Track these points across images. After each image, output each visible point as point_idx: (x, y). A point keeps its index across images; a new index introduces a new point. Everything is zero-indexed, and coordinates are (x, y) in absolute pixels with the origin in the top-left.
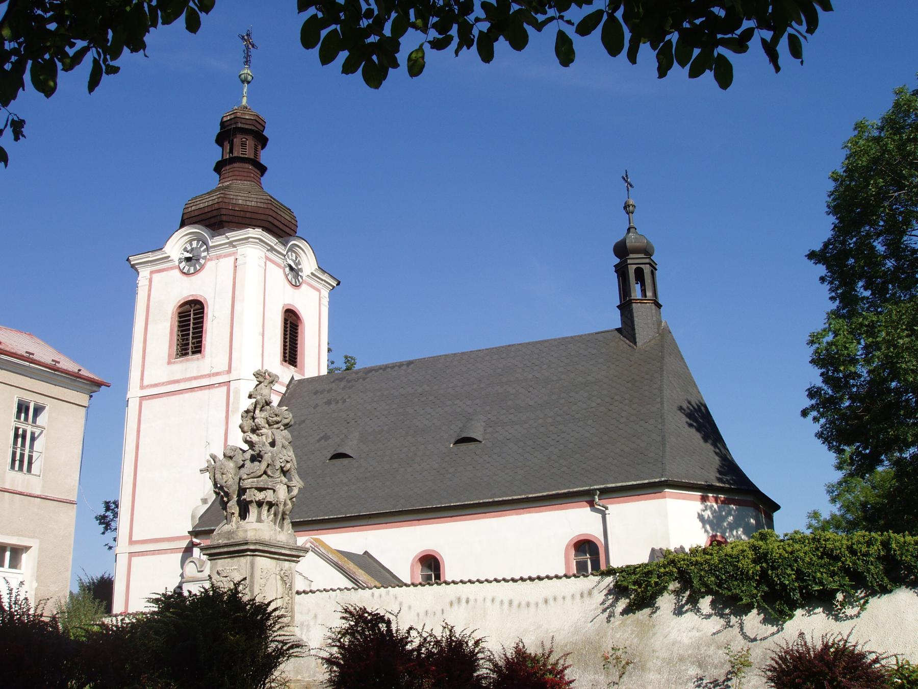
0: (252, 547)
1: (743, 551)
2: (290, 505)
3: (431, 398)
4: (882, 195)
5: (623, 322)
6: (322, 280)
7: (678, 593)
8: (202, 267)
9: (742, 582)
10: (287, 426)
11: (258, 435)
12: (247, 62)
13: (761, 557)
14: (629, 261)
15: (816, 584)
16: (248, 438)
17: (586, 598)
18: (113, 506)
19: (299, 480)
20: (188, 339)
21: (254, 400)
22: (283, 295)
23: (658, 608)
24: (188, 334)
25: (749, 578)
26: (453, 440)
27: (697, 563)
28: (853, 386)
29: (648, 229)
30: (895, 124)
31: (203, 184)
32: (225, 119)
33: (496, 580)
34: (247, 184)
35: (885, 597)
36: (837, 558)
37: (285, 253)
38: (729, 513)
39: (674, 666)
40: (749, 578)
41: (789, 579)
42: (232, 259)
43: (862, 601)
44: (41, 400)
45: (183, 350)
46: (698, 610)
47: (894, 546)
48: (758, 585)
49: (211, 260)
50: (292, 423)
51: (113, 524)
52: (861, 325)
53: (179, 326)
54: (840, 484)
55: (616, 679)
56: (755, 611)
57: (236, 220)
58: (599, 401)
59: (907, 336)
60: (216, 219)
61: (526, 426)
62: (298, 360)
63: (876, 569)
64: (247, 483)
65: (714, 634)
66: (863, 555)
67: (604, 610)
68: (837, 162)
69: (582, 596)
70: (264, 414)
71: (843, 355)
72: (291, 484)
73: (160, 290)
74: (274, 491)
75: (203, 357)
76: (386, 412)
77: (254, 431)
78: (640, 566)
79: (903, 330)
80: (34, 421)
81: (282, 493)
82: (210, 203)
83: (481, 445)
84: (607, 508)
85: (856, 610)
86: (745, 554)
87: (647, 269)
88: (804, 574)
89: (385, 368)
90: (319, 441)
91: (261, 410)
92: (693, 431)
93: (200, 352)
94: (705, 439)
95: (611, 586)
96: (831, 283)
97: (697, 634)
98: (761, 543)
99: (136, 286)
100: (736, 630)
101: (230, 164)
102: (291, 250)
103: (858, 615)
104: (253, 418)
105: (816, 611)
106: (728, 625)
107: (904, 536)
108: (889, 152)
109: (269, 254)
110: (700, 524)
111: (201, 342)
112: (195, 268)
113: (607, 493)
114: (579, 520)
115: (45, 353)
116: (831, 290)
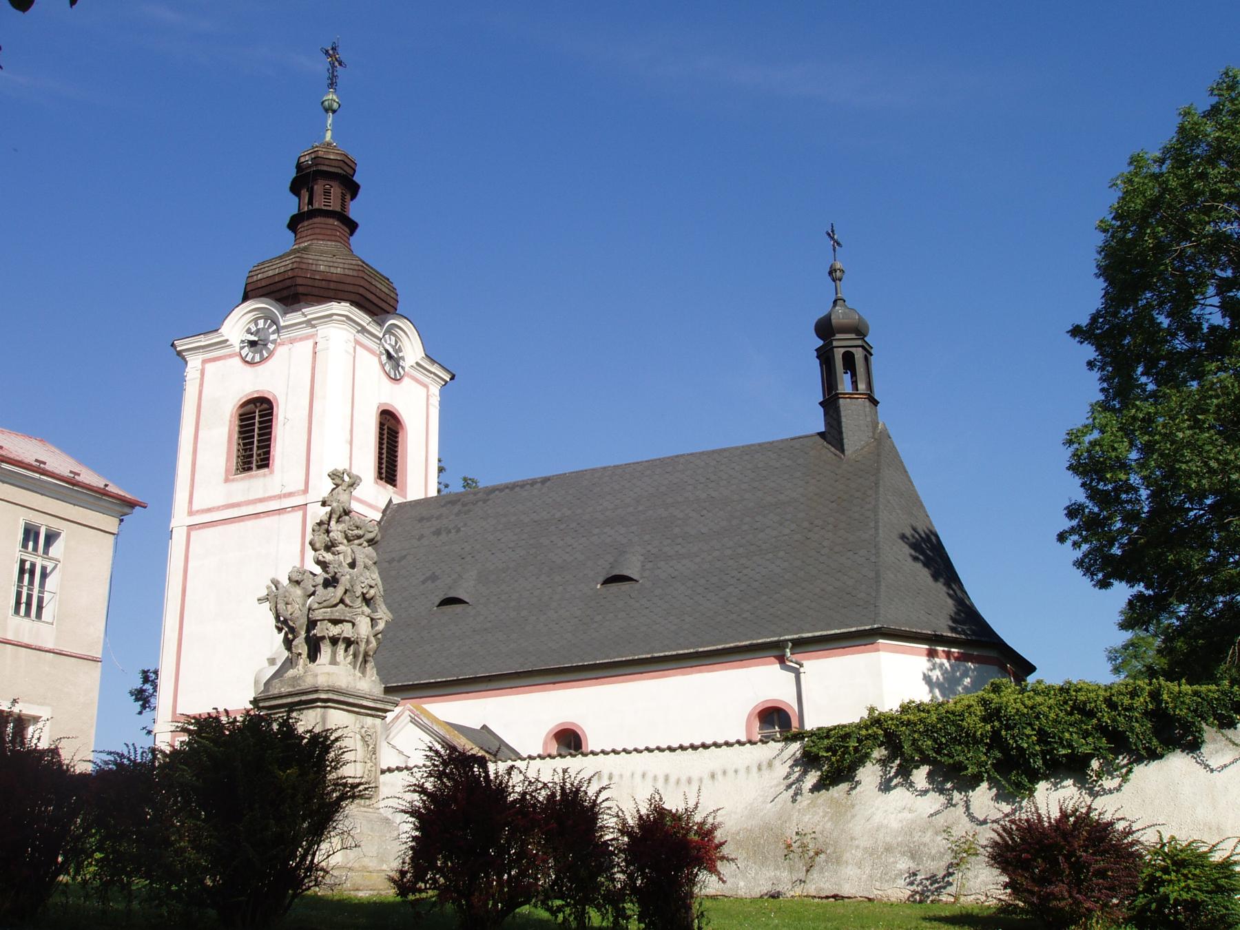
0: (323, 696)
1: (970, 706)
2: (374, 644)
3: (573, 525)
4: (1161, 249)
5: (827, 424)
6: (431, 372)
7: (884, 762)
8: (271, 353)
9: (967, 746)
10: (371, 542)
11: (333, 554)
12: (332, 84)
13: (992, 714)
14: (835, 344)
15: (1064, 747)
16: (321, 558)
17: (765, 772)
18: (153, 676)
19: (386, 611)
20: (251, 449)
21: (328, 509)
22: (378, 391)
23: (858, 783)
24: (252, 443)
25: (976, 742)
26: (601, 579)
27: (909, 723)
28: (1127, 502)
29: (860, 302)
30: (1180, 155)
31: (275, 245)
32: (302, 160)
33: (648, 750)
34: (330, 245)
35: (1154, 765)
36: (1091, 714)
37: (381, 335)
38: (965, 674)
39: (879, 857)
40: (976, 742)
41: (1027, 741)
42: (310, 343)
43: (1124, 770)
44: (55, 524)
45: (244, 463)
46: (911, 785)
47: (1165, 697)
48: (988, 751)
50: (378, 538)
51: (152, 700)
52: (1134, 418)
53: (240, 432)
54: (1125, 647)
55: (802, 875)
56: (985, 785)
57: (315, 291)
58: (793, 526)
59: (1190, 428)
60: (289, 291)
61: (698, 560)
62: (399, 478)
63: (1142, 728)
64: (317, 615)
65: (932, 815)
66: (1126, 709)
67: (789, 786)
68: (1103, 202)
69: (759, 768)
70: (341, 527)
71: (1110, 459)
72: (376, 616)
73: (215, 386)
74: (354, 625)
75: (272, 472)
76: (512, 545)
77: (328, 548)
78: (835, 728)
79: (1183, 421)
80: (46, 551)
81: (364, 628)
82: (282, 270)
83: (637, 586)
84: (801, 666)
85: (1117, 781)
86: (972, 709)
87: (859, 354)
88: (1047, 734)
89: (512, 487)
90: (423, 582)
91: (338, 521)
92: (919, 565)
93: (267, 466)
94: (936, 577)
95: (798, 755)
96: (1102, 369)
97: (910, 816)
98: (992, 695)
99: (180, 381)
100: (961, 809)
101: (308, 219)
102: (389, 331)
103: (1118, 789)
104: (328, 532)
105: (1065, 783)
106: (950, 804)
107: (1179, 685)
108: (1171, 191)
109: (360, 337)
110: (927, 688)
111: (268, 453)
112: (262, 355)
113: (801, 645)
114: (764, 682)
115: (60, 463)
116: (1102, 379)
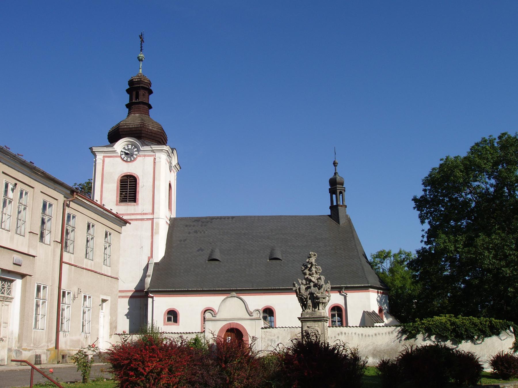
3: (251, 237)
8: (135, 159)
17: (391, 335)
25: (449, 330)
29: (343, 174)
35: (489, 338)
36: (477, 326)
42: (152, 158)
46: (431, 340)
49: (140, 156)
69: (389, 333)
75: (138, 204)
85: (480, 342)
89: (221, 218)
90: (198, 251)
103: (481, 343)
113: (347, 288)
